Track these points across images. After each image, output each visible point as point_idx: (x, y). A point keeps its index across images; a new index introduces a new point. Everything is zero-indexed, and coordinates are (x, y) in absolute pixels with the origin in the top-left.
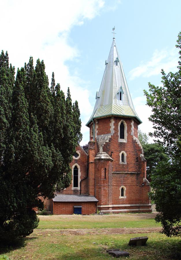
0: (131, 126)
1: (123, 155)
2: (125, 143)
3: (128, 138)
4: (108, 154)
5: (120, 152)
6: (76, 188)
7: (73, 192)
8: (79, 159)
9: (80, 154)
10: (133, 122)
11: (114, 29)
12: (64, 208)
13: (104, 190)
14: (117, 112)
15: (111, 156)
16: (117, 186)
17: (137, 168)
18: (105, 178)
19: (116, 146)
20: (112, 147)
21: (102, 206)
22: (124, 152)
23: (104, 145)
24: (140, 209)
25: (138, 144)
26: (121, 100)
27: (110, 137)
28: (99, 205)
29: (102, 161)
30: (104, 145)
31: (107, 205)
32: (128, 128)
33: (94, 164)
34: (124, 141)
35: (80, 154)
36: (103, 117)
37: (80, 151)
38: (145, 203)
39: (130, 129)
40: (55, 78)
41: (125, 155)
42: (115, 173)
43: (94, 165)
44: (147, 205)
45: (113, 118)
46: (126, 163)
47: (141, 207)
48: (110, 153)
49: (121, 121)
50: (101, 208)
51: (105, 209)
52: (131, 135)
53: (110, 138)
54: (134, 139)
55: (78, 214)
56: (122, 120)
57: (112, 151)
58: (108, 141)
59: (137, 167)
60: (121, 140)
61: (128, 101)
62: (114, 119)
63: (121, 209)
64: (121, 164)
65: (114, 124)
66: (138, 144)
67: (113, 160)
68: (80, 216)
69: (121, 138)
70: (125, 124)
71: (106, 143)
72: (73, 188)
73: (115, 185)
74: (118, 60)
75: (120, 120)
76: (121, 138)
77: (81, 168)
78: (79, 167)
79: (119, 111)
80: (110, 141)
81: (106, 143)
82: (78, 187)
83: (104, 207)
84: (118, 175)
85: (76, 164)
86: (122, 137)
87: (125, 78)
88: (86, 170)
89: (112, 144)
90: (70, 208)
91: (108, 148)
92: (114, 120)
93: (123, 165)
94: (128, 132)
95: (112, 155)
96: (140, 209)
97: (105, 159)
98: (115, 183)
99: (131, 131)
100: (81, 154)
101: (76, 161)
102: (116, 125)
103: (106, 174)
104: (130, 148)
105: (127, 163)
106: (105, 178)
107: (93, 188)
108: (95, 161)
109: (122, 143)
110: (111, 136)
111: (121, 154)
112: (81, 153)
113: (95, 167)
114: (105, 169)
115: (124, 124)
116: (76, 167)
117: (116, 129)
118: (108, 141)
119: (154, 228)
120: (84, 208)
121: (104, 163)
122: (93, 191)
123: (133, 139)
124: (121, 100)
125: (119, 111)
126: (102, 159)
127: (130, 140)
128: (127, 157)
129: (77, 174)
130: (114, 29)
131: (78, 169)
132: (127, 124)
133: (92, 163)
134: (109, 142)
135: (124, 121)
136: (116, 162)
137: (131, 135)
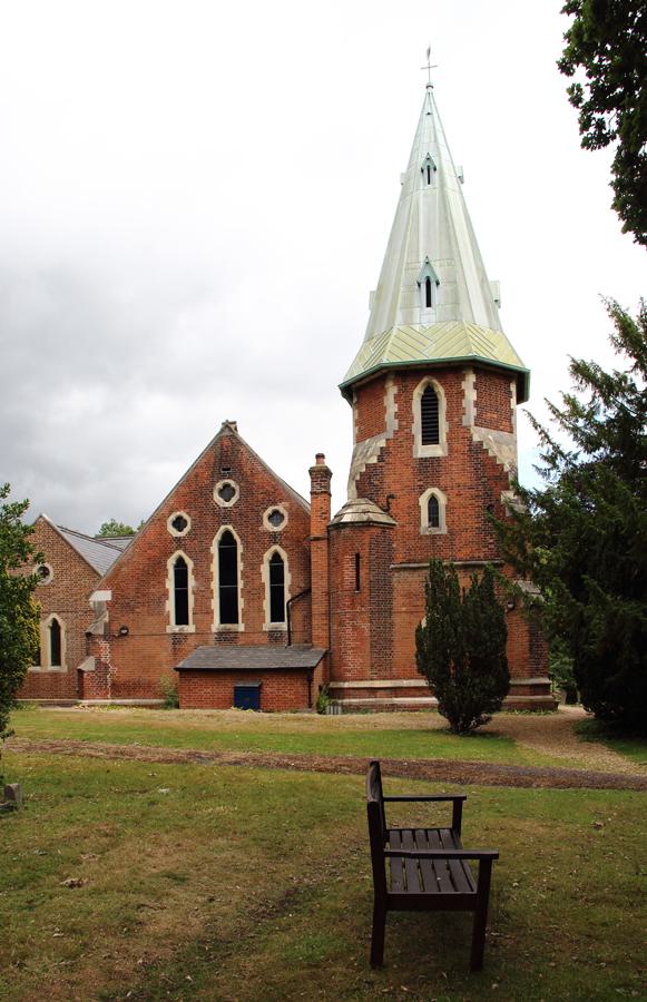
0: (461, 394)
2: (438, 459)
3: (449, 439)
4: (376, 503)
6: (229, 626)
7: (265, 639)
9: (286, 514)
10: (471, 378)
12: (382, 692)
15: (386, 510)
16: (412, 612)
17: (492, 546)
18: (358, 588)
19: (408, 473)
20: (393, 477)
21: (346, 685)
22: (436, 491)
23: (361, 474)
25: (491, 454)
26: (429, 304)
27: (382, 443)
28: (341, 681)
29: (346, 531)
30: (361, 474)
32: (448, 401)
33: (325, 543)
34: (437, 451)
35: (286, 514)
36: (424, 367)
37: (287, 504)
39: (459, 404)
40: (470, 212)
41: (442, 500)
42: (405, 569)
43: (325, 548)
45: (393, 377)
46: (443, 529)
48: (383, 500)
50: (342, 689)
52: (464, 424)
53: (382, 448)
54: (476, 438)
55: (244, 709)
56: (425, 380)
57: (392, 493)
58: (374, 460)
59: (491, 541)
60: (423, 451)
62: (394, 380)
63: (414, 696)
64: (427, 533)
65: (397, 398)
66: (491, 454)
67: (394, 525)
68: (250, 713)
69: (425, 442)
70: (440, 390)
71: (367, 466)
72: (268, 625)
73: (404, 609)
76: (425, 442)
77: (290, 561)
78: (284, 555)
79: (406, 347)
80: (380, 459)
81: (367, 466)
82: (187, 623)
83: (353, 689)
84: (416, 574)
85: (276, 547)
86: (430, 436)
87: (467, 218)
90: (226, 689)
91: (376, 483)
92: (395, 385)
93: (434, 537)
94: (449, 418)
95: (393, 507)
97: (352, 523)
98: (404, 605)
100: (290, 515)
102: (404, 400)
104: (460, 474)
105: (451, 532)
106: (358, 588)
107: (325, 622)
109: (426, 459)
110: (387, 440)
111: (423, 501)
113: (329, 554)
114: (358, 556)
117: (404, 415)
118: (374, 460)
120: (271, 688)
122: (325, 634)
123: (470, 439)
124: (429, 304)
125: (406, 347)
126: (346, 524)
128: (447, 506)
129: (185, 584)
131: (282, 561)
133: (317, 539)
134: (381, 464)
135: (435, 381)
136: (409, 528)
137: (464, 424)
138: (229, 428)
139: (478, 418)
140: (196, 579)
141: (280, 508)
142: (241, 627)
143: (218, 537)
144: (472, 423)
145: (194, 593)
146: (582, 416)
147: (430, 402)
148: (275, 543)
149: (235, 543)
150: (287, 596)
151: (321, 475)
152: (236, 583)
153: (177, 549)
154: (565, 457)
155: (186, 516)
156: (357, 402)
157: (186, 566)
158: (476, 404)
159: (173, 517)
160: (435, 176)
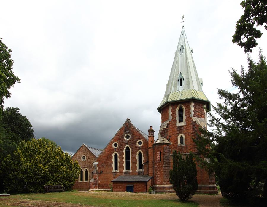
0: (190, 108)
1: (182, 137)
4: (166, 138)
5: (178, 135)
6: (128, 170)
8: (142, 146)
10: (193, 104)
11: (183, 18)
13: (159, 171)
14: (175, 97)
15: (169, 140)
21: (157, 186)
22: (182, 134)
24: (202, 190)
25: (198, 124)
26: (181, 85)
27: (168, 123)
31: (163, 185)
33: (152, 149)
35: (142, 142)
37: (143, 139)
38: (206, 184)
41: (184, 137)
43: (152, 150)
44: (206, 186)
45: (170, 105)
46: (184, 145)
47: (203, 188)
49: (179, 106)
51: (160, 188)
56: (180, 105)
58: (165, 127)
60: (179, 124)
61: (189, 84)
62: (171, 106)
65: (172, 111)
66: (198, 124)
69: (179, 122)
74: (183, 47)
75: (178, 105)
76: (179, 122)
78: (142, 152)
80: (167, 127)
81: (164, 129)
88: (147, 155)
89: (170, 129)
90: (124, 187)
91: (166, 133)
93: (182, 147)
96: (202, 190)
99: (189, 113)
100: (144, 142)
101: (140, 148)
102: (174, 111)
103: (162, 157)
107: (152, 169)
108: (153, 146)
111: (179, 137)
112: (143, 141)
115: (183, 108)
116: (140, 153)
117: (174, 115)
118: (165, 127)
119: (70, 195)
121: (158, 148)
124: (181, 85)
127: (189, 122)
130: (183, 18)
132: (185, 107)
133: (150, 148)
135: (182, 105)
138: (258, 44)
139: (194, 115)
140: (120, 159)
141: (141, 140)
142: (131, 171)
143: (125, 148)
144: (193, 116)
145: (119, 162)
146: (223, 109)
147: (181, 111)
148: (140, 149)
149: (130, 149)
150: (143, 163)
151: (151, 132)
152: (130, 160)
153: (115, 151)
154: (216, 120)
155: (117, 143)
156: (162, 113)
157: (117, 156)
158: (194, 111)
159: (114, 143)
160: (184, 51)
